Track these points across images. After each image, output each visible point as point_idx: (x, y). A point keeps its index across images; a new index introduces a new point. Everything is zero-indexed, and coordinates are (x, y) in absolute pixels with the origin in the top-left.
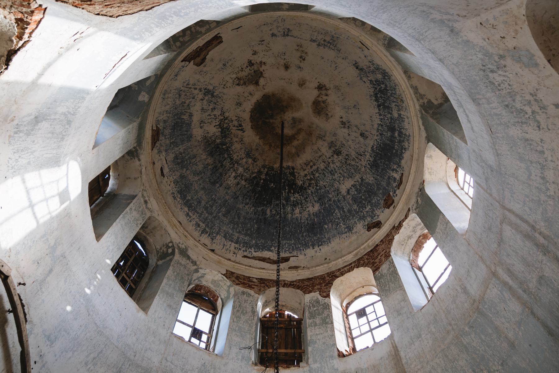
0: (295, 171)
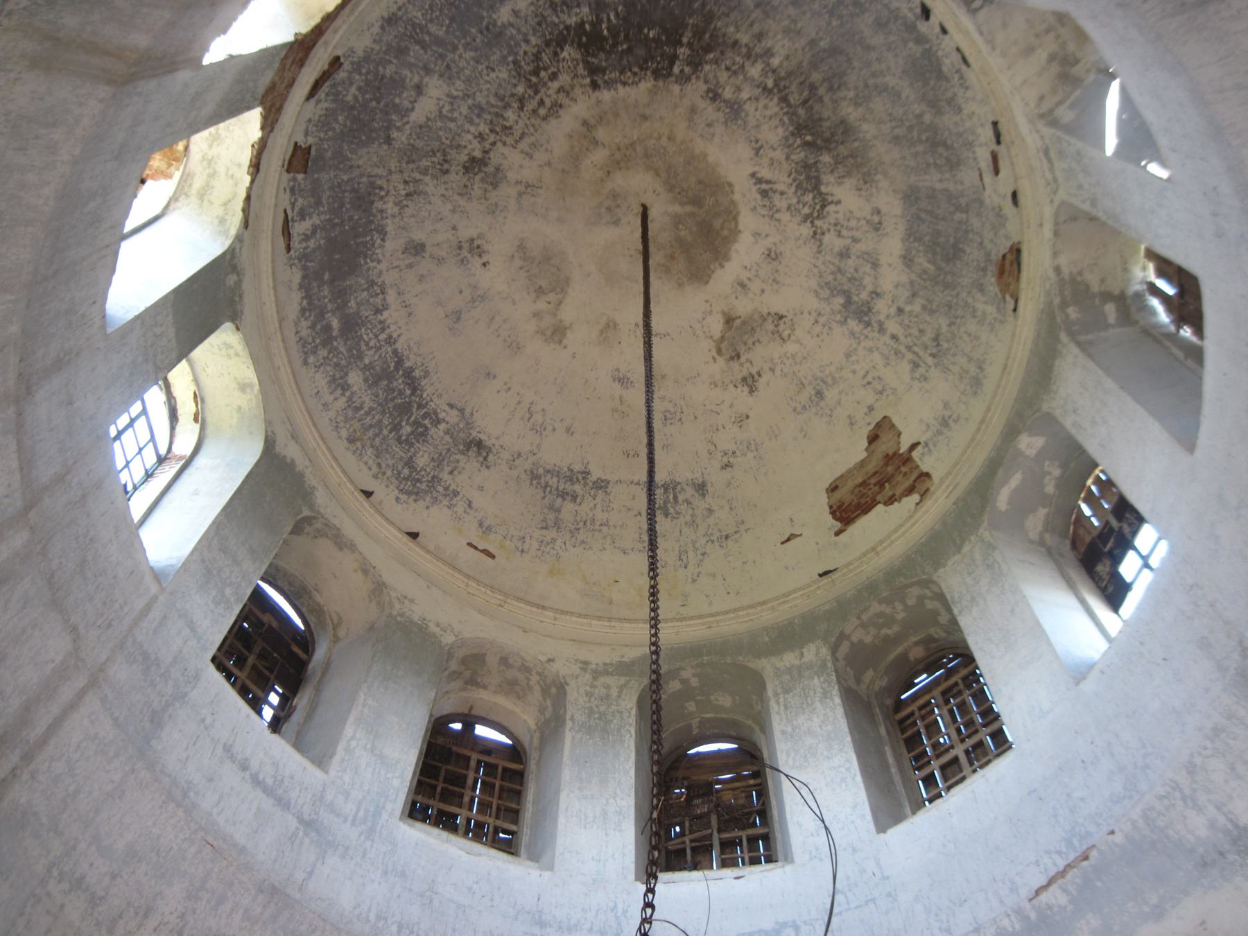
0: (588, 80)
